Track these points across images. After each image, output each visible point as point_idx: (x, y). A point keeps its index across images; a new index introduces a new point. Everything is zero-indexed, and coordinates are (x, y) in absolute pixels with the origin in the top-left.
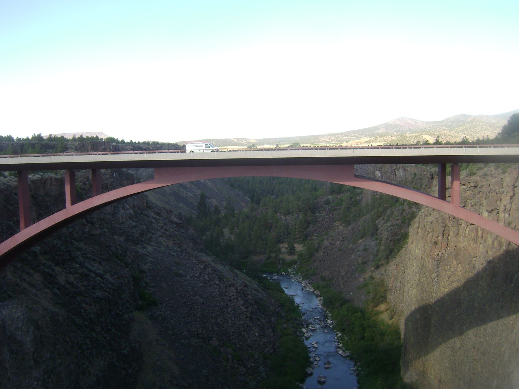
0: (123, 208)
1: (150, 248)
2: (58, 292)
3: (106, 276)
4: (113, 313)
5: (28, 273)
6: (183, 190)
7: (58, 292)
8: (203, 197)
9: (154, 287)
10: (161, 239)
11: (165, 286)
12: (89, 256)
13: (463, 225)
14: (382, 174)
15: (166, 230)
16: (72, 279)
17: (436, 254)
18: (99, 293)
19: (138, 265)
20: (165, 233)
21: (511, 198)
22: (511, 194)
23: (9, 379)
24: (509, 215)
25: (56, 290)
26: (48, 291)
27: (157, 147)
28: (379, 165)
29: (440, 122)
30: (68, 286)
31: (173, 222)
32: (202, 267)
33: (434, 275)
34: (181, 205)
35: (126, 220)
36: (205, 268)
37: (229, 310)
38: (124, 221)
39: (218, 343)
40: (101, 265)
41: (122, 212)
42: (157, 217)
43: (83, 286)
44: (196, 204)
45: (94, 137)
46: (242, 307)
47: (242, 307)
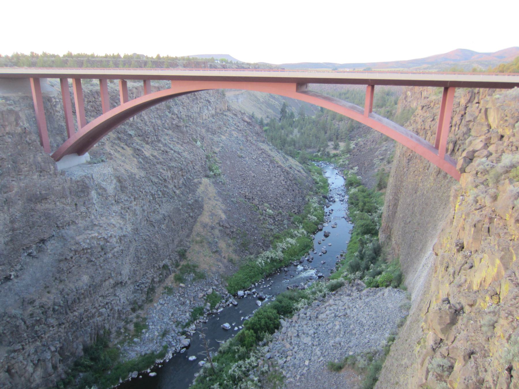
0: (208, 109)
1: (223, 138)
2: (142, 161)
3: (184, 154)
4: (185, 177)
5: (123, 148)
6: (271, 100)
7: (142, 161)
8: (285, 106)
9: (220, 163)
10: (233, 132)
11: (229, 163)
12: (174, 140)
13: (429, 134)
14: (412, 94)
15: (238, 126)
16: (155, 154)
17: (408, 154)
18: (173, 164)
19: (212, 148)
20: (237, 129)
21: (462, 116)
22: (463, 112)
23: (96, 210)
24: (459, 129)
25: (140, 159)
26: (135, 159)
27: (270, 68)
28: (411, 87)
29: (494, 53)
30: (151, 157)
31: (245, 121)
32: (260, 152)
33: (405, 170)
34: (270, 110)
35: (209, 118)
36: (261, 153)
37: (273, 182)
38: (207, 118)
39: (258, 203)
40: (182, 146)
41: (206, 111)
42: (234, 117)
43: (163, 158)
44: (280, 110)
45: (39, 55)
46: (282, 181)
47: (282, 181)
